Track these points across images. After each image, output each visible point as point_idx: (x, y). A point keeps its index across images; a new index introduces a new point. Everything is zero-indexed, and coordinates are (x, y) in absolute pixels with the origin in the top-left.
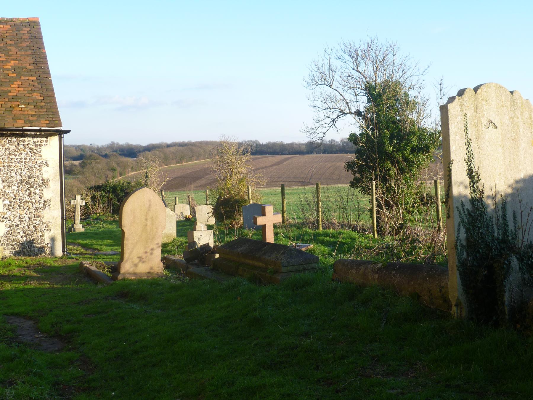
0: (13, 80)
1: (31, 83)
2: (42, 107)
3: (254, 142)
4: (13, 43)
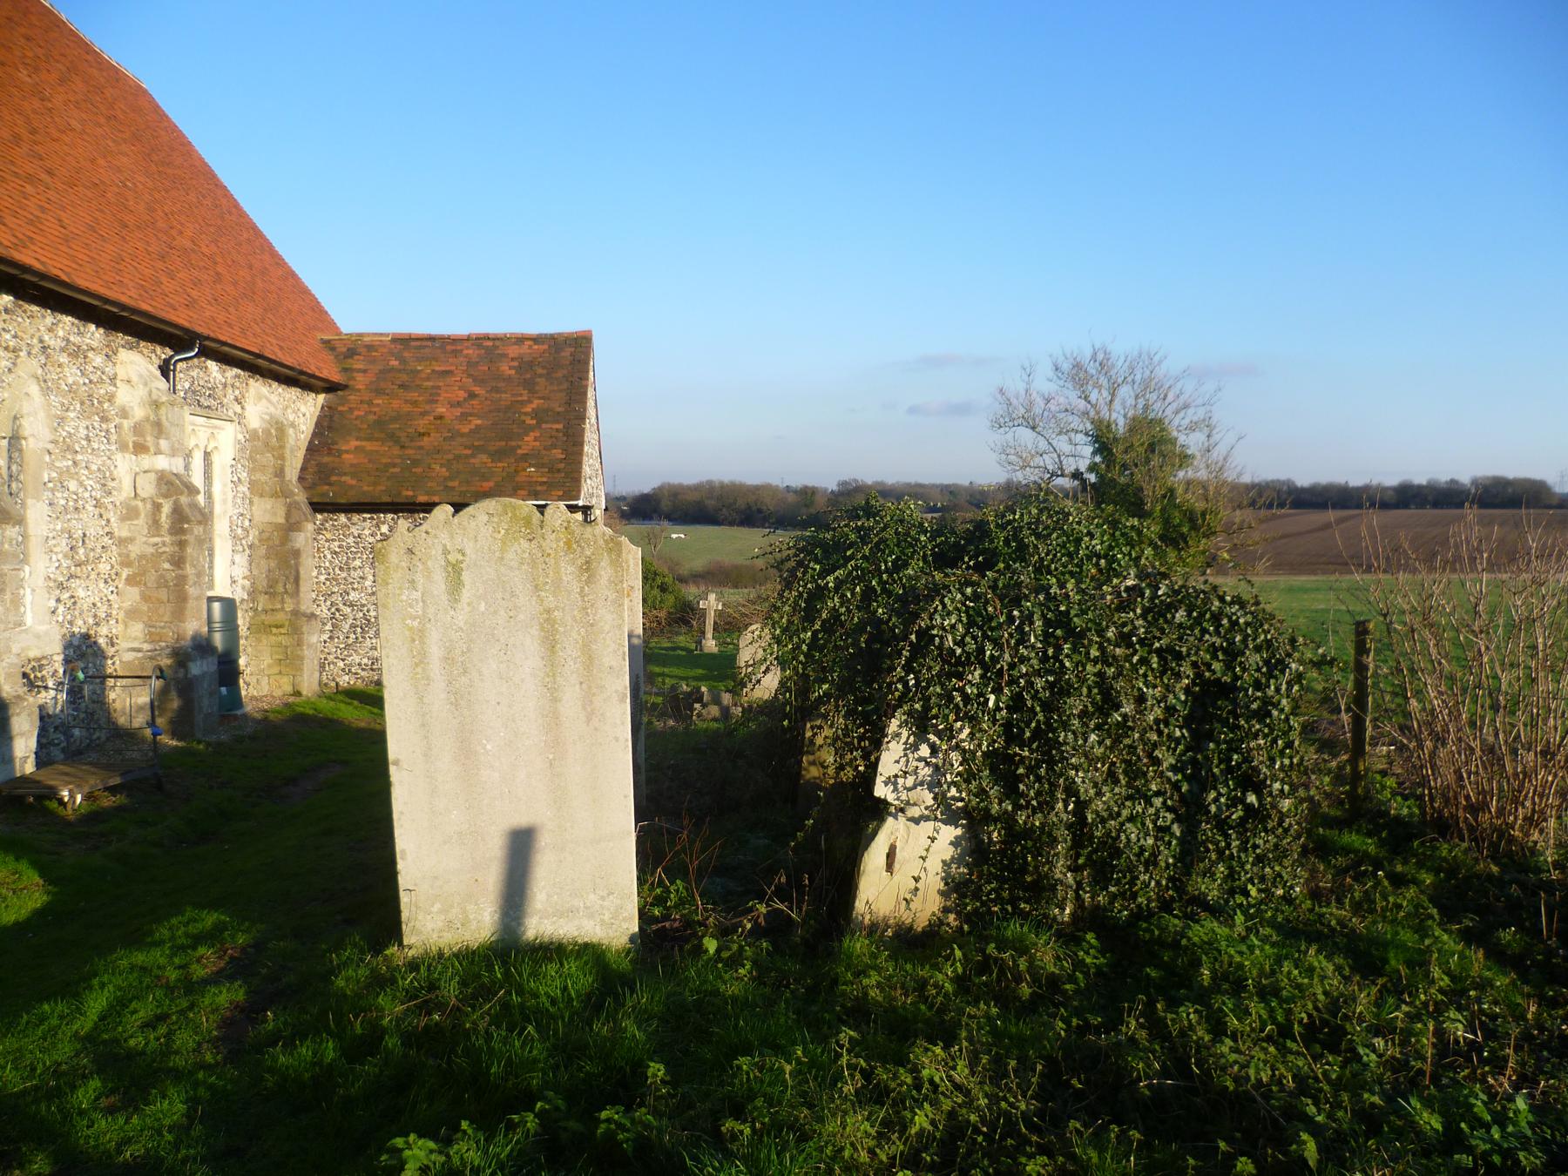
0: (531, 428)
1: (554, 433)
2: (559, 471)
3: (1283, 483)
4: (545, 372)
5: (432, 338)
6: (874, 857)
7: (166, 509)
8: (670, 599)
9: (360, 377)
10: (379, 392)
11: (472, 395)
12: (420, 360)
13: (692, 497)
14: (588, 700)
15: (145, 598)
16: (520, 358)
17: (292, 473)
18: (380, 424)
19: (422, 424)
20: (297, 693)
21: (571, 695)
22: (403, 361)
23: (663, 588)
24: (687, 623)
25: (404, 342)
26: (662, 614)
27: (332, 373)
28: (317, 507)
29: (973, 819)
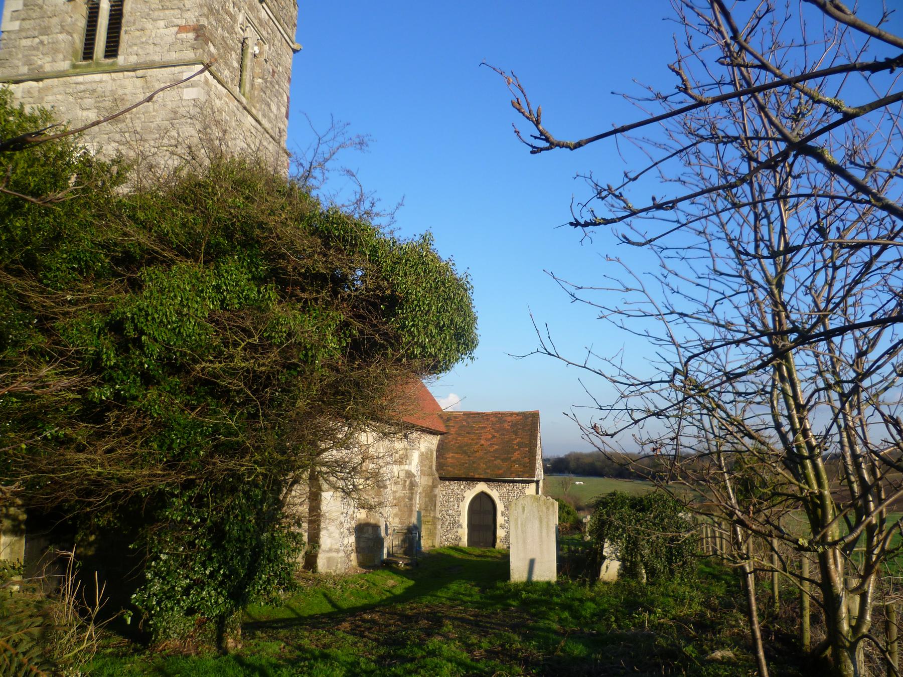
0: (517, 450)
5: (478, 414)
6: (604, 567)
7: (408, 482)
8: (571, 518)
9: (452, 429)
10: (459, 435)
11: (494, 437)
12: (474, 422)
13: (587, 461)
14: (548, 533)
15: (400, 510)
16: (511, 422)
17: (434, 468)
18: (460, 447)
19: (476, 447)
20: (434, 546)
21: (544, 532)
22: (468, 422)
23: (568, 513)
24: (579, 529)
25: (468, 415)
26: (568, 525)
27: (442, 429)
28: (443, 479)
29: (623, 560)
